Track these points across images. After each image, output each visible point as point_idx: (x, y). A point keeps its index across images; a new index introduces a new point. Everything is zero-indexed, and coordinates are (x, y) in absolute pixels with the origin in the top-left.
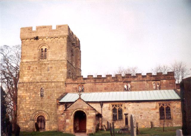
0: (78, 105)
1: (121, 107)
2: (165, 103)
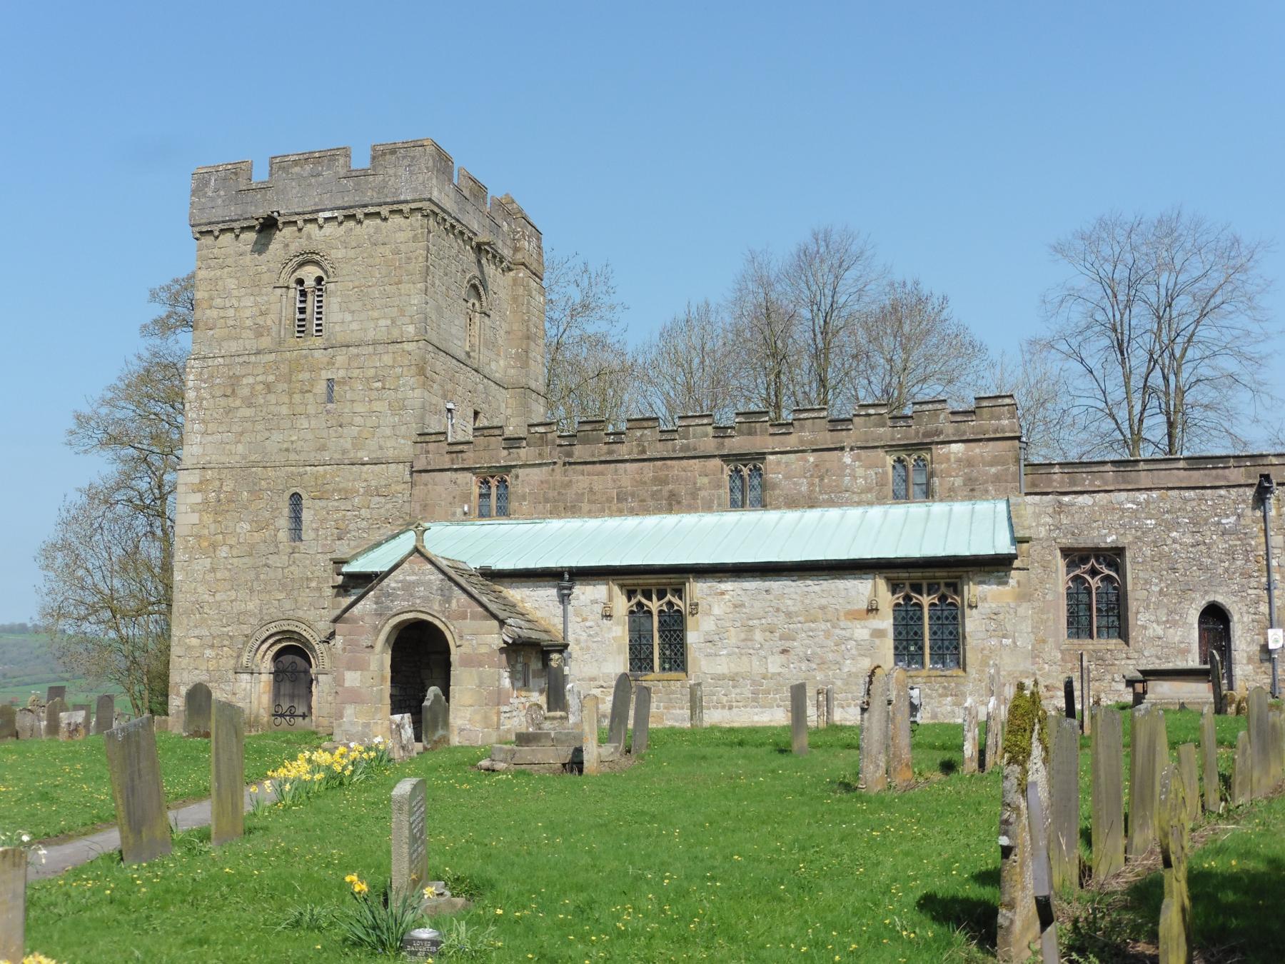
0: (408, 587)
1: (676, 600)
2: (924, 578)
